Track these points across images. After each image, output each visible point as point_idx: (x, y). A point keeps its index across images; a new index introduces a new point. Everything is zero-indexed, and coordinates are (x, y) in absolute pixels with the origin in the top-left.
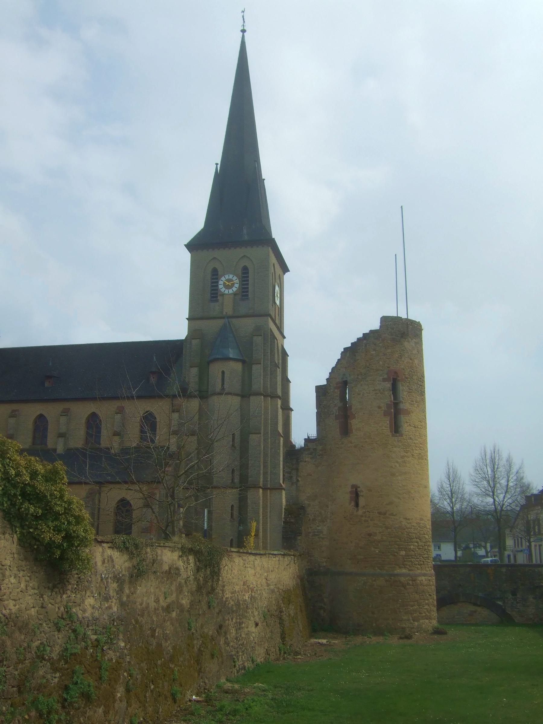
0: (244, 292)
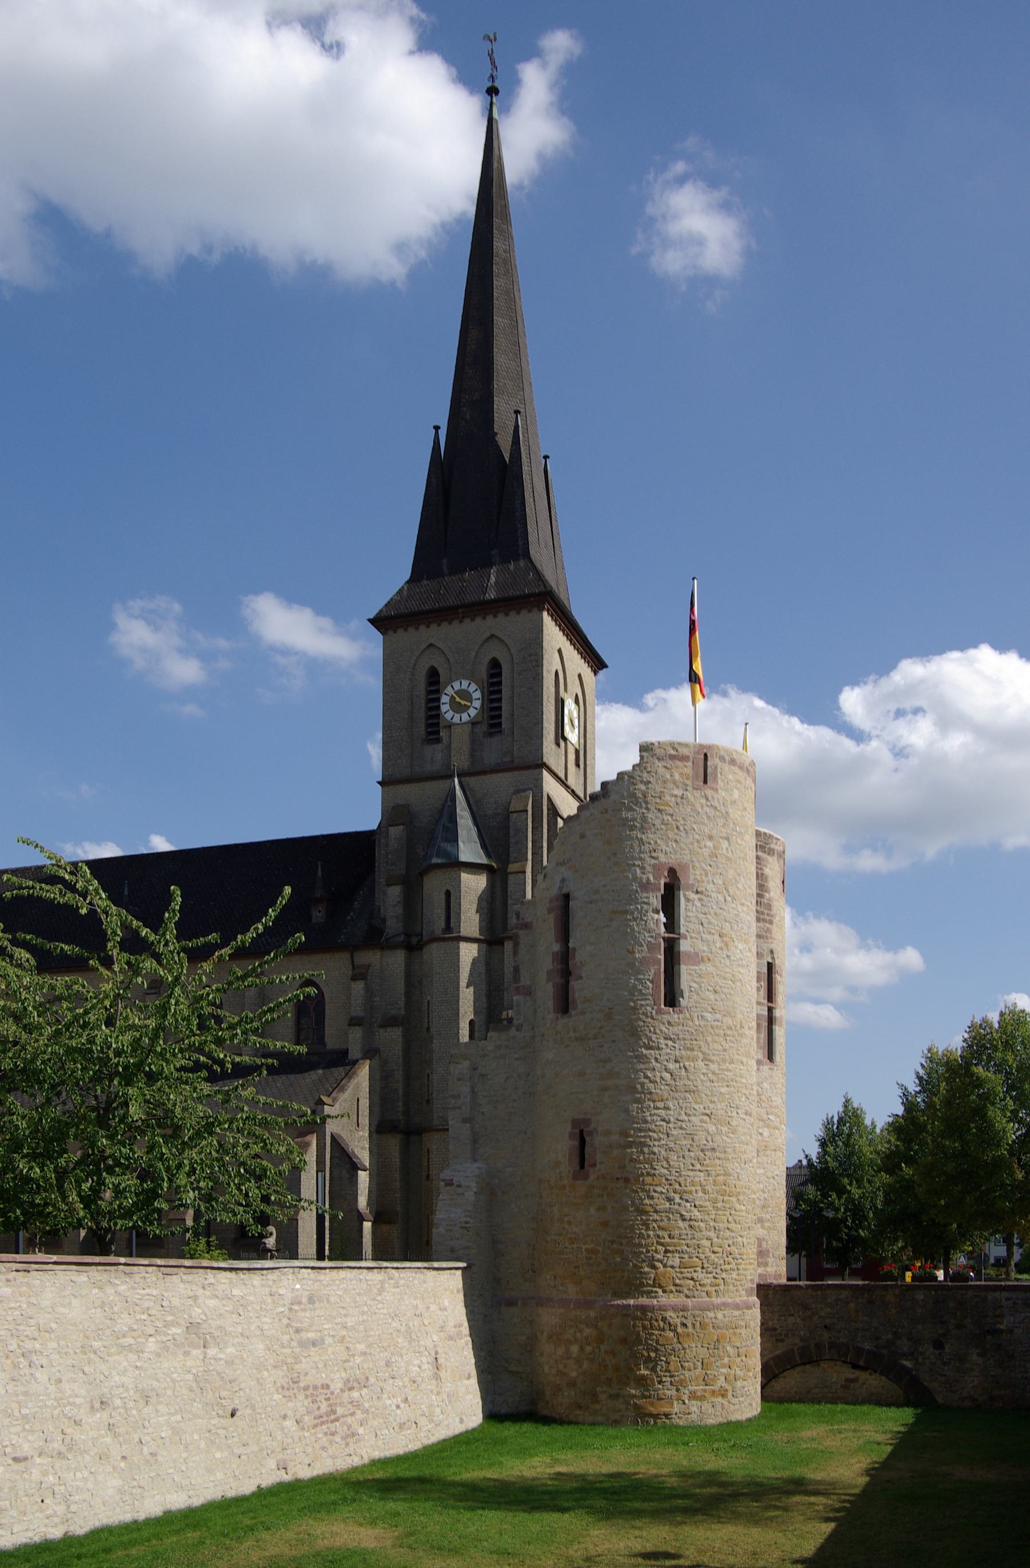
0: (493, 717)
